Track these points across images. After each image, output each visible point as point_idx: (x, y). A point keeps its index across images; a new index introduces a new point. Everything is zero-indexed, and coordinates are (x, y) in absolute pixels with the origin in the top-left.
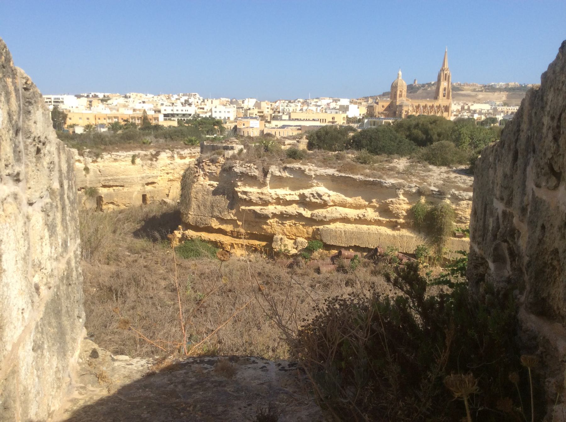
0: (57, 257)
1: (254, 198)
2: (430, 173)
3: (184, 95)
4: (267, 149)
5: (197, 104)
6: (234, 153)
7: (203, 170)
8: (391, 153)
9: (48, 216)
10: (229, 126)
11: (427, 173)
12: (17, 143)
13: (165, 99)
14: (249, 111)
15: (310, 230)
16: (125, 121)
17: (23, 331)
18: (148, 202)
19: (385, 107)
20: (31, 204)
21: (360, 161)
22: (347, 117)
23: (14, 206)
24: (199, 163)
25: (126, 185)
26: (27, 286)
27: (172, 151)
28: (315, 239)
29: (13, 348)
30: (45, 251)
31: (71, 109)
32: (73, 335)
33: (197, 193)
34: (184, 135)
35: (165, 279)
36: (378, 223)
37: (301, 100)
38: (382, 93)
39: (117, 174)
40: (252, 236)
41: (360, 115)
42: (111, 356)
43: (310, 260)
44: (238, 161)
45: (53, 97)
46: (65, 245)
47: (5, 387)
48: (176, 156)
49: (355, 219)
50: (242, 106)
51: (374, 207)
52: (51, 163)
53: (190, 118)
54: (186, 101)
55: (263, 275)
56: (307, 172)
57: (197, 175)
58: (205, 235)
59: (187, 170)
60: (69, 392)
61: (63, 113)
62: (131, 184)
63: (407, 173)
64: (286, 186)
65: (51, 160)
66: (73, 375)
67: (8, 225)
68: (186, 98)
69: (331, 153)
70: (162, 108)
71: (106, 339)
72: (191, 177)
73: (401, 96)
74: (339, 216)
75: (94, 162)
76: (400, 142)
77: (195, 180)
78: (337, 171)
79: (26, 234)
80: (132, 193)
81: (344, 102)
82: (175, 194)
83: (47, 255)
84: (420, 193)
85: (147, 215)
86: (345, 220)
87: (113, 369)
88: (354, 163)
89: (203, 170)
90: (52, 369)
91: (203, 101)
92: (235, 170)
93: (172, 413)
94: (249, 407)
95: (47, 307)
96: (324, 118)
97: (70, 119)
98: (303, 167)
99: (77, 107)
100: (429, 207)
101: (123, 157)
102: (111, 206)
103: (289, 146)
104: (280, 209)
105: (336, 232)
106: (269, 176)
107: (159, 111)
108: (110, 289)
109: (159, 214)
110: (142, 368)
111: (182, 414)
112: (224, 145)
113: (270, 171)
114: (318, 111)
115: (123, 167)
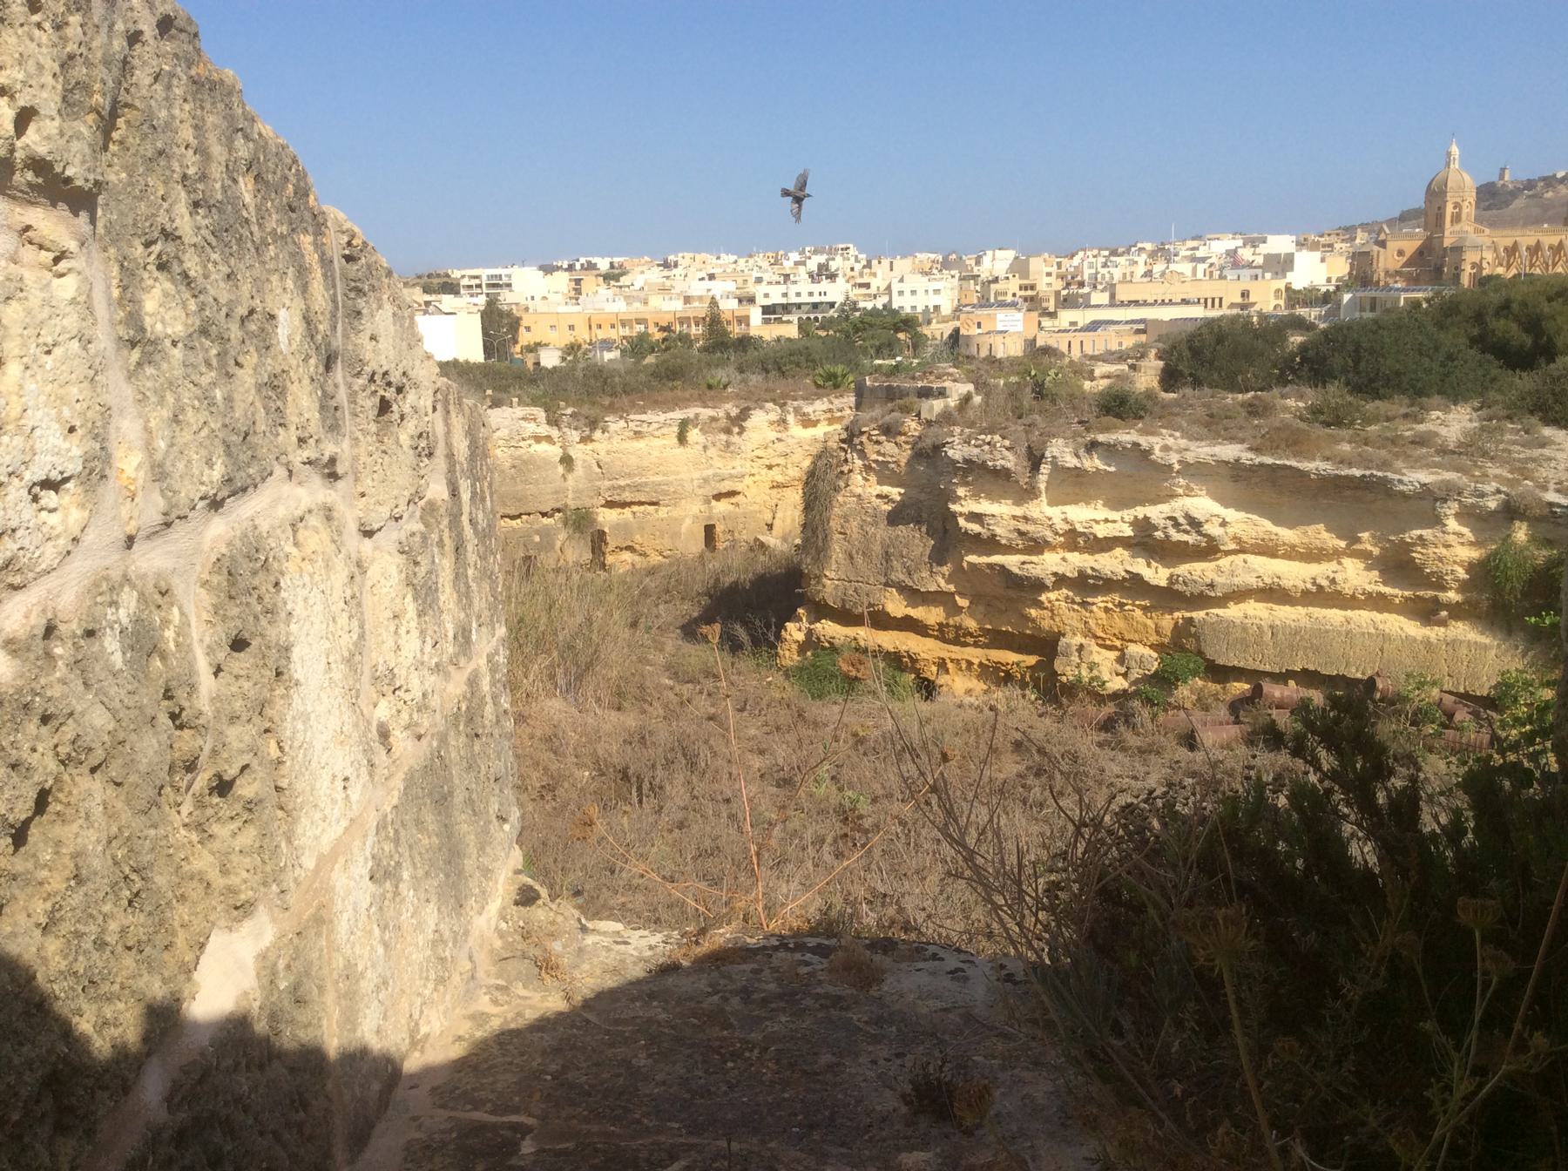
0: (437, 665)
1: (1002, 532)
2: (1546, 452)
3: (815, 252)
4: (1040, 392)
5: (850, 274)
6: (946, 406)
7: (862, 454)
8: (1420, 393)
9: (416, 563)
10: (937, 331)
11: (1536, 452)
12: (330, 389)
13: (765, 264)
14: (993, 286)
15: (1167, 622)
16: (663, 329)
17: (346, 829)
18: (720, 546)
19: (1408, 254)
20: (369, 534)
21: (1322, 418)
22: (1288, 288)
23: (325, 535)
24: (851, 437)
25: (664, 499)
26: (356, 725)
27: (782, 406)
28: (1182, 649)
29: (317, 865)
30: (405, 647)
31: (530, 304)
32: (485, 860)
33: (846, 518)
34: (813, 361)
35: (761, 752)
36: (1378, 602)
37: (1149, 246)
38: (1397, 215)
39: (642, 470)
40: (998, 640)
41: (1329, 280)
42: (579, 920)
43: (1165, 710)
44: (957, 430)
45: (485, 273)
46: (464, 637)
47: (296, 949)
48: (791, 418)
49: (1306, 593)
50: (976, 272)
51: (1364, 555)
52: (420, 435)
53: (832, 313)
54: (823, 268)
55: (1028, 750)
56: (1157, 453)
57: (845, 469)
58: (865, 635)
59: (819, 457)
60: (469, 996)
61: (509, 314)
62: (677, 498)
63: (1469, 451)
64: (1096, 498)
65: (420, 430)
66: (482, 958)
67: (307, 578)
68: (822, 259)
69: (1231, 398)
70: (759, 291)
71: (612, 902)
72: (831, 476)
73: (1457, 218)
74: (1252, 582)
75: (585, 440)
76: (1450, 357)
77: (842, 484)
78: (1251, 449)
79: (353, 603)
80: (679, 521)
81: (1280, 244)
82: (789, 521)
83: (411, 656)
84: (1511, 511)
85: (717, 580)
86: (1273, 593)
87: (581, 950)
88: (1303, 425)
89: (862, 454)
90: (423, 931)
91: (869, 265)
92: (950, 453)
93: (705, 1061)
94: (899, 1062)
95: (410, 782)
96: (1217, 295)
97: (528, 329)
98: (1144, 442)
99: (545, 298)
100: (1542, 555)
101: (655, 426)
102: (627, 556)
103: (1106, 382)
104: (1077, 561)
105: (1244, 629)
106: (1045, 469)
107: (752, 300)
108: (625, 775)
109: (746, 578)
110: (650, 953)
111: (730, 1064)
112: (920, 384)
113: (1048, 454)
114: (1200, 275)
115: (656, 453)
